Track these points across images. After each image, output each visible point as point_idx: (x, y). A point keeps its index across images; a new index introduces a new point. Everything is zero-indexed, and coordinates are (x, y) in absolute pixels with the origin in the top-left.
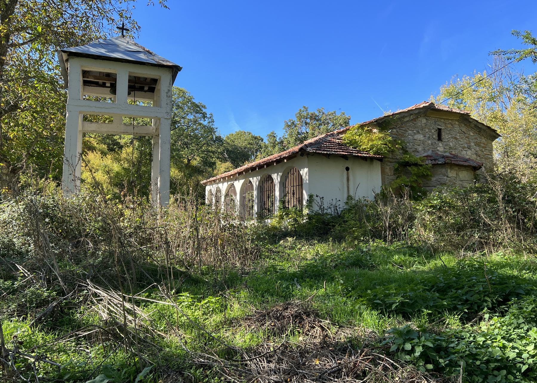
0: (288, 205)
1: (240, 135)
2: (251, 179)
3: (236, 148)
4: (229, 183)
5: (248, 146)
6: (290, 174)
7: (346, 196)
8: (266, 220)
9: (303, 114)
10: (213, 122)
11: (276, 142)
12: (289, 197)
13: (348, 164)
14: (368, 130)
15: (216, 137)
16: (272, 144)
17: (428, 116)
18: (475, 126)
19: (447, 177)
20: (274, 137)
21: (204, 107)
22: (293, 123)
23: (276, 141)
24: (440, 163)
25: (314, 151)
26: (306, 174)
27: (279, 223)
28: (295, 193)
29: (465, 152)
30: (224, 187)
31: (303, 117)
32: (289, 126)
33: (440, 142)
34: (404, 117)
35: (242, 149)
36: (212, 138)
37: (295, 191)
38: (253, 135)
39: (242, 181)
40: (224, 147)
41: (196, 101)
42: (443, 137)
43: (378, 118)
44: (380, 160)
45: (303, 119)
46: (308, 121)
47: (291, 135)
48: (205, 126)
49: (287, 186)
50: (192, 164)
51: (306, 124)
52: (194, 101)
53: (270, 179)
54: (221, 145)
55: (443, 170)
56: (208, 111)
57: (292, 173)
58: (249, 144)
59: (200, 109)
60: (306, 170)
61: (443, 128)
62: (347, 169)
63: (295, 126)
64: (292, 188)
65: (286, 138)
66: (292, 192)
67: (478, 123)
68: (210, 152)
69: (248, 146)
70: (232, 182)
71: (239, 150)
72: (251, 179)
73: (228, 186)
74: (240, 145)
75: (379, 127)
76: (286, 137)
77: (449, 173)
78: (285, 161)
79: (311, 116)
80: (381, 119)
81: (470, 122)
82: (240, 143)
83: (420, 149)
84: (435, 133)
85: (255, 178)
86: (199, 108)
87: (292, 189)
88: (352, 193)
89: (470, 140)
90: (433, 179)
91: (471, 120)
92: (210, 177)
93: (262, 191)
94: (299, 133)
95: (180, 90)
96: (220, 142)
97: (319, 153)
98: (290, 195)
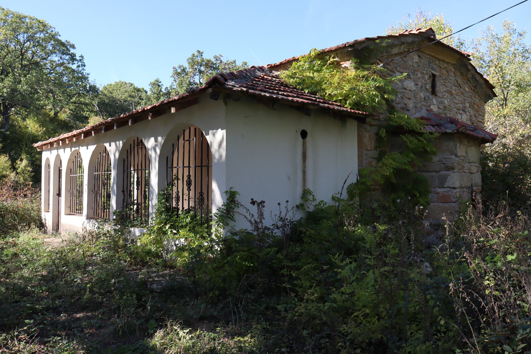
0: (177, 203)
1: (119, 85)
2: (107, 145)
3: (114, 101)
4: (73, 149)
5: (129, 99)
6: (181, 141)
7: (299, 191)
8: (132, 229)
9: (197, 59)
10: (84, 66)
11: (161, 93)
12: (180, 187)
13: (306, 124)
14: (332, 63)
15: (90, 87)
16: (155, 95)
17: (422, 52)
18: (473, 76)
19: (456, 156)
20: (159, 86)
21: (73, 47)
22: (184, 70)
23: (161, 91)
24: (448, 131)
25: (245, 89)
26: (220, 145)
27: (158, 242)
28: (193, 183)
29: (460, 116)
30: (65, 154)
31: (196, 63)
32: (178, 74)
33: (434, 96)
34: (392, 46)
35: (121, 102)
36: (85, 87)
37: (192, 178)
38: (136, 86)
39: (92, 148)
40: (100, 98)
41: (63, 39)
42: (437, 89)
43: (361, 37)
44: (361, 120)
45: (196, 67)
46: (202, 68)
47: (181, 85)
48: (73, 71)
49: (175, 165)
50: (60, 118)
51: (200, 72)
52: (59, 38)
53: (141, 144)
54: (96, 97)
55: (452, 144)
56: (77, 52)
57: (187, 138)
58: (130, 96)
59: (67, 49)
60: (221, 134)
61: (437, 74)
62: (304, 134)
63: (186, 74)
64: (186, 170)
65: (174, 88)
66: (186, 178)
67: (476, 74)
68: (82, 104)
69: (129, 99)
70: (78, 148)
71: (117, 103)
72: (107, 145)
73: (71, 155)
74: (118, 97)
75: (356, 57)
76: (175, 87)
77: (458, 150)
78: (173, 110)
79: (206, 63)
80: (356, 43)
81: (468, 70)
82: (119, 95)
83: (411, 105)
84: (428, 81)
85: (113, 144)
86: (66, 47)
87: (186, 174)
88: (310, 186)
89: (465, 98)
90: (436, 159)
91: (470, 68)
92: (49, 138)
93: (126, 169)
94: (190, 83)
95: (40, 23)
96: (95, 93)
97: (254, 95)
98: (180, 182)
